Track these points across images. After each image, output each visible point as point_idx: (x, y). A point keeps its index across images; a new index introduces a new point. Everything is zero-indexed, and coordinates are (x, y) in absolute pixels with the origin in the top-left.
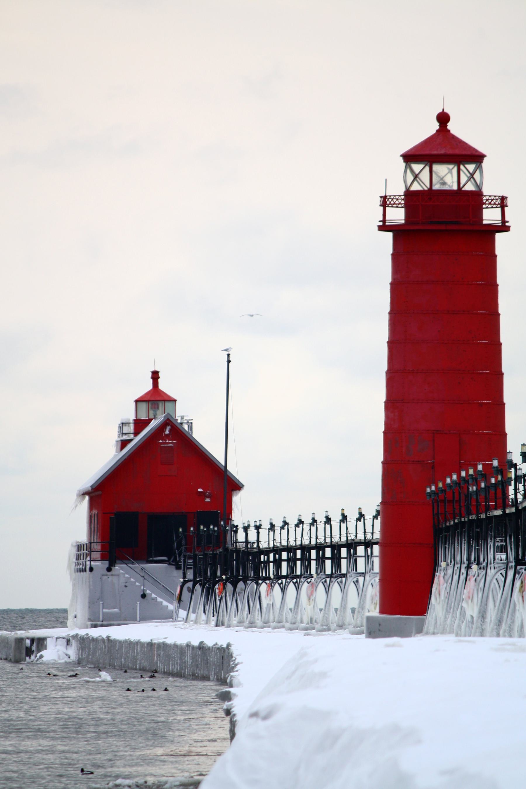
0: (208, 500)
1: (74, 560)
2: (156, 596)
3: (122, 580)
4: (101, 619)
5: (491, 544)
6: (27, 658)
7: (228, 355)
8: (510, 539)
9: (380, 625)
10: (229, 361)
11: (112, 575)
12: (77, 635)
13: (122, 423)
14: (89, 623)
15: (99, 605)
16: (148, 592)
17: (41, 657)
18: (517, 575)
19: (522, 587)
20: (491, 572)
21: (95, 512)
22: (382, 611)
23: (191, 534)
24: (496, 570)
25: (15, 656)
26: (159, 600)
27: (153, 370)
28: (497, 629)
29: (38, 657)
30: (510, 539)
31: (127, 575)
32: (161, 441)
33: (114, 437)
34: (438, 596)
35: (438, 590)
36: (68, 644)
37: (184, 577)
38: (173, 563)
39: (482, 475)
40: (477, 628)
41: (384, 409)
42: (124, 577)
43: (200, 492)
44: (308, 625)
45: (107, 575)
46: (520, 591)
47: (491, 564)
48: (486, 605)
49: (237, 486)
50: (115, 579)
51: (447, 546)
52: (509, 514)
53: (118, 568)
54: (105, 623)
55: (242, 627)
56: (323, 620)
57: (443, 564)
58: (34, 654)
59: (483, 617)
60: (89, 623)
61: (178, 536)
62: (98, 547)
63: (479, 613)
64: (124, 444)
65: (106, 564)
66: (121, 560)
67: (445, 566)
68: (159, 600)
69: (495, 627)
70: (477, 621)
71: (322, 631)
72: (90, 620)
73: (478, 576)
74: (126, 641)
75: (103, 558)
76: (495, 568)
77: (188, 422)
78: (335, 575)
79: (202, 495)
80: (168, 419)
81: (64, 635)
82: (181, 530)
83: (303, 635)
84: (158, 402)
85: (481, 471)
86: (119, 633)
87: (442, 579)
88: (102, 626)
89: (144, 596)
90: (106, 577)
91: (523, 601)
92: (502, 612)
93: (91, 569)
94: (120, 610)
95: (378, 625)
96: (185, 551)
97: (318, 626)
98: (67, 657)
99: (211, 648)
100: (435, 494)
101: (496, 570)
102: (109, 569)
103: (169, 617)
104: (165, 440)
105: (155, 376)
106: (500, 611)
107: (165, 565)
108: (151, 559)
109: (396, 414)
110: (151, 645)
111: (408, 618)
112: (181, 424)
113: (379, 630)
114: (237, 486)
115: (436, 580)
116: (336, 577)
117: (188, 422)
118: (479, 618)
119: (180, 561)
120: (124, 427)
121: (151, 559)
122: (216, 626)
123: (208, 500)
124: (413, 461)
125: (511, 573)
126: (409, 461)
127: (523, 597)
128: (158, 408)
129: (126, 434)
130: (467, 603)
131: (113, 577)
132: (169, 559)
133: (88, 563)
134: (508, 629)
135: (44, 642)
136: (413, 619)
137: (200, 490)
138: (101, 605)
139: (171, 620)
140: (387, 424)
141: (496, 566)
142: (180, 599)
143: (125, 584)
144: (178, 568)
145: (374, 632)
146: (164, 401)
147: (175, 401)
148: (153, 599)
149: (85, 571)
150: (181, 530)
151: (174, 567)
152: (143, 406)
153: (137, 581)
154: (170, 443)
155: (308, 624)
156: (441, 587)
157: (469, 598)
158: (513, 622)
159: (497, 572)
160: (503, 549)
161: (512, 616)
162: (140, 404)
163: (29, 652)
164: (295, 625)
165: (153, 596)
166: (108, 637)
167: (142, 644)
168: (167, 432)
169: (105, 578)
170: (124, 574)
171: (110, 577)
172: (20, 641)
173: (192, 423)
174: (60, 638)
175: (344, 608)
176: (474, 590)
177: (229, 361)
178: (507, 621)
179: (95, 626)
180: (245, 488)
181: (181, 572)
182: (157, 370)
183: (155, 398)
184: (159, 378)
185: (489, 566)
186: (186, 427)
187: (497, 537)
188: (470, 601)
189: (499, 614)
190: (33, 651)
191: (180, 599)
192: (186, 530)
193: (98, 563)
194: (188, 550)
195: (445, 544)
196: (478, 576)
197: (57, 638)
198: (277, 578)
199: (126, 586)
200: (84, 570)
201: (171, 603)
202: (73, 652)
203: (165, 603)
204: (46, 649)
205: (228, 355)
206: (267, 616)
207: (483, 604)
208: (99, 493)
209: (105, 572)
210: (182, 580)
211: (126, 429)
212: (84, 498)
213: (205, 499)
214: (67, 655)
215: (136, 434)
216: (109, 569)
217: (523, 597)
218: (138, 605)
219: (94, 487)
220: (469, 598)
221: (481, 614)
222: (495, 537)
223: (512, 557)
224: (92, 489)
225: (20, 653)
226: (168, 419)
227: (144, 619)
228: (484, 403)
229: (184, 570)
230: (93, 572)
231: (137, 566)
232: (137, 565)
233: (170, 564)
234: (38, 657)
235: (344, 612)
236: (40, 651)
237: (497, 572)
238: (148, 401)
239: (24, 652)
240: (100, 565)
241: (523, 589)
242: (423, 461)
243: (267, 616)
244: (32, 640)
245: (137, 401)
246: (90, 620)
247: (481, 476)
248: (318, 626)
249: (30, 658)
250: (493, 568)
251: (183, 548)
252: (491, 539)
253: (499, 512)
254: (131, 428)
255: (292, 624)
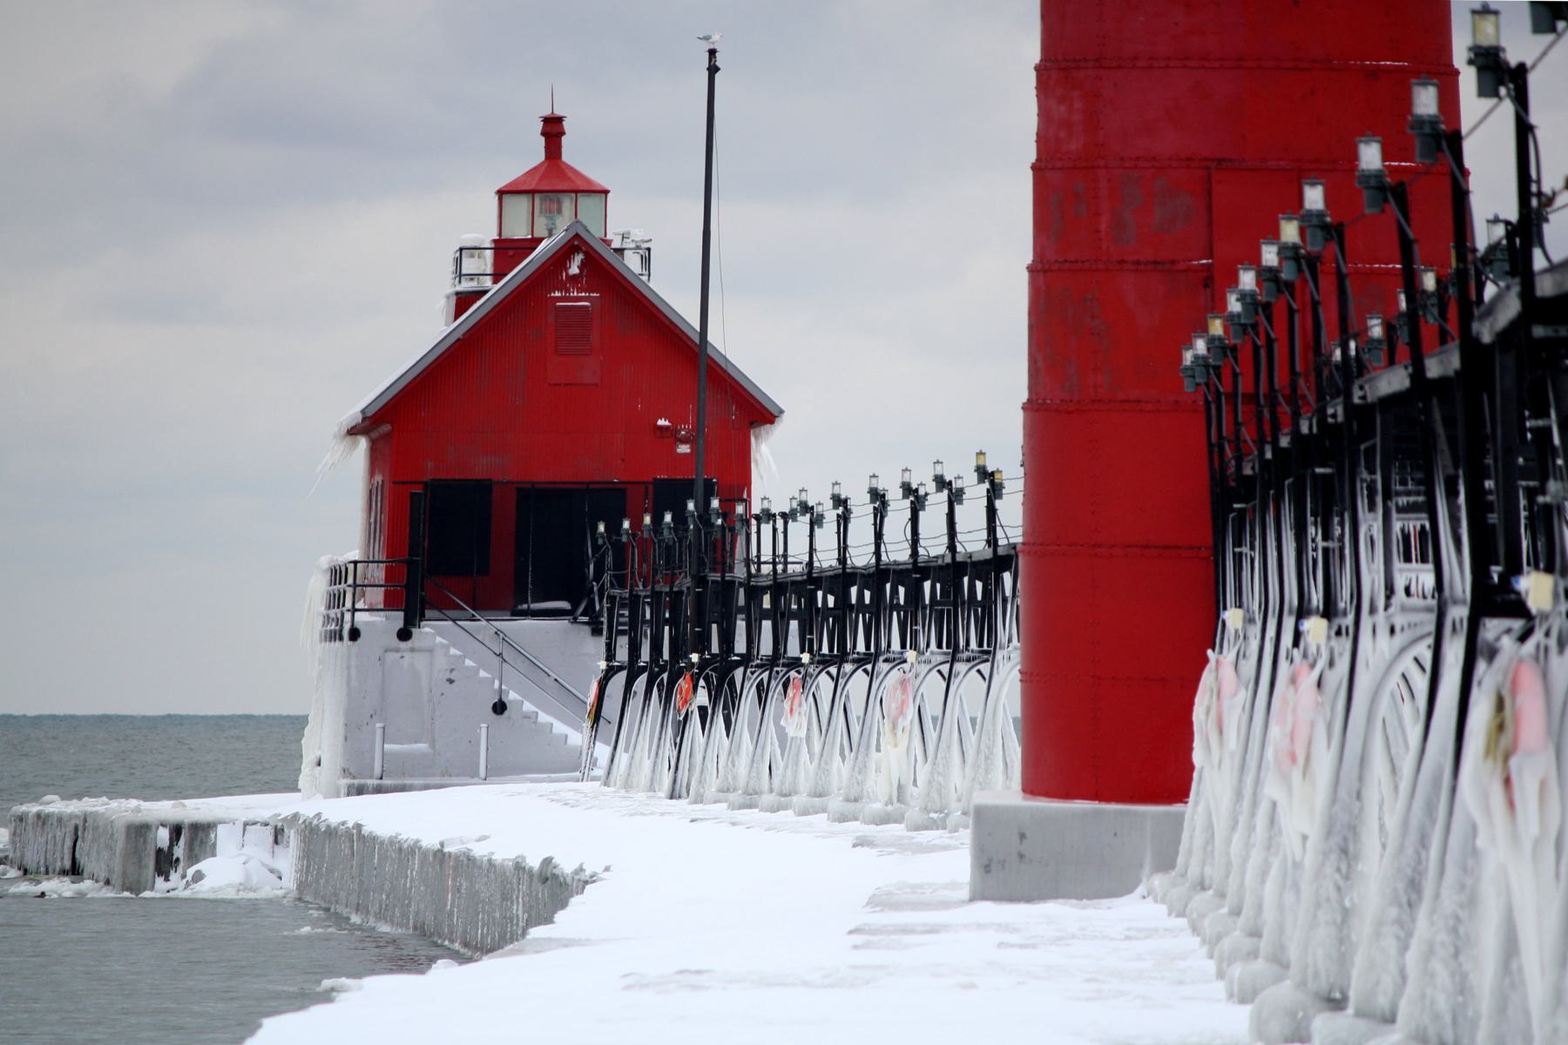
0: (684, 449)
1: (322, 609)
2: (534, 709)
3: (441, 663)
4: (377, 771)
5: (1371, 524)
6: (160, 881)
7: (712, 53)
8: (1452, 494)
9: (1022, 836)
10: (713, 70)
11: (412, 650)
12: (296, 816)
13: (461, 249)
14: (344, 782)
15: (374, 733)
16: (512, 696)
17: (198, 877)
18: (1481, 666)
19: (1501, 727)
20: (1376, 648)
21: (378, 478)
22: (1033, 787)
23: (624, 539)
24: (1400, 639)
25: (124, 873)
26: (544, 718)
27: (547, 112)
28: (1399, 922)
29: (189, 877)
30: (1452, 494)
31: (453, 651)
32: (557, 294)
33: (447, 287)
34: (1214, 737)
35: (1213, 713)
36: (276, 842)
37: (610, 656)
38: (586, 619)
39: (1325, 227)
40: (1318, 906)
41: (1034, 92)
42: (447, 655)
43: (661, 428)
44: (890, 808)
45: (397, 650)
46: (1489, 751)
47: (1373, 610)
48: (1359, 796)
49: (760, 414)
50: (420, 661)
51: (1245, 550)
52: (1443, 381)
53: (430, 632)
54: (386, 782)
55: (725, 805)
56: (928, 794)
57: (1232, 617)
58: (180, 869)
59: (1344, 851)
60: (344, 782)
61: (594, 541)
62: (378, 573)
63: (1329, 832)
64: (463, 301)
65: (397, 619)
66: (440, 610)
67: (1239, 625)
68: (544, 718)
69: (1393, 912)
70: (1318, 873)
71: (926, 828)
72: (346, 772)
73: (1331, 664)
74: (392, 841)
75: (390, 604)
76: (1392, 631)
77: (638, 248)
78: (965, 655)
79: (671, 435)
80: (577, 236)
81: (264, 814)
82: (601, 528)
83: (850, 840)
84: (561, 196)
85: (1320, 214)
86: (396, 817)
87: (1227, 671)
88: (379, 790)
89: (500, 708)
90: (398, 655)
91: (1511, 804)
92: (1424, 842)
93: (355, 634)
94: (433, 744)
95: (1016, 838)
96: (612, 586)
97: (914, 813)
98: (273, 877)
99: (569, 880)
100: (1207, 366)
101: (1400, 639)
102: (404, 635)
103: (571, 765)
104: (567, 290)
105: (553, 129)
106: (1413, 836)
107: (562, 624)
108: (525, 606)
109: (1078, 105)
110: (440, 855)
111: (1128, 812)
112: (620, 251)
113: (1021, 856)
114: (760, 414)
115: (1207, 677)
116: (968, 660)
117: (638, 248)
118: (1326, 854)
119: (600, 613)
120: (465, 261)
121: (525, 606)
122: (672, 797)
123: (684, 449)
124: (1138, 263)
125: (1454, 652)
126: (1122, 262)
127: (1507, 782)
128: (560, 211)
129: (472, 276)
130: (1286, 779)
131: (415, 655)
132: (575, 606)
133: (348, 616)
134: (1443, 937)
135: (208, 835)
136: (1144, 814)
137: (662, 422)
138: (379, 733)
139: (577, 774)
140: (1042, 139)
141: (1399, 621)
142: (597, 716)
143: (448, 675)
144: (597, 632)
145: (1003, 863)
146: (576, 192)
147: (606, 192)
148: (527, 716)
149: (341, 638)
150: (601, 528)
151: (587, 629)
152: (519, 207)
153: (481, 665)
154: (582, 299)
155: (890, 802)
156: (1226, 703)
157: (1293, 758)
158: (1471, 902)
159: (1403, 650)
160: (1426, 547)
161: (1465, 869)
162: (506, 198)
163: (165, 863)
164: (858, 805)
165: (528, 707)
166: (358, 826)
167: (425, 854)
168: (574, 269)
169: (392, 657)
170: (447, 648)
171: (408, 656)
172: (140, 831)
173: (649, 249)
174: (255, 823)
175: (987, 758)
176: (1313, 725)
177: (713, 70)
178: (1437, 895)
179: (360, 791)
180: (785, 417)
181: (602, 642)
182: (558, 112)
183: (553, 180)
184: (563, 133)
185: (1366, 621)
186: (632, 262)
187: (1398, 494)
188: (1296, 774)
189: (1410, 851)
190: (178, 860)
191: (597, 716)
192: (614, 528)
193: (378, 618)
194: (620, 582)
195: (1238, 542)
196: (1331, 664)
197: (246, 824)
198: (819, 662)
199: (451, 681)
200: (336, 636)
201: (578, 728)
202: (288, 861)
203: (560, 728)
204: (214, 855)
205: (712, 53)
206: (789, 772)
207: (1342, 793)
208: (386, 428)
209: (395, 641)
210: (603, 665)
211: (469, 266)
212: (355, 445)
213: (674, 446)
214: (272, 871)
215: (497, 277)
216: (404, 635)
217: (1507, 782)
218: (484, 731)
219: (370, 413)
220: (1293, 758)
221: (1336, 840)
222: (1387, 496)
223: (1460, 580)
224: (364, 419)
225: (140, 865)
226: (577, 236)
227: (499, 770)
228: (1387, 70)
229: (610, 637)
230: (359, 641)
231: (484, 627)
232: (484, 623)
233: (575, 621)
234: (189, 877)
235: (987, 771)
236: (198, 861)
237: (1403, 650)
238: (532, 192)
239: (151, 863)
240: (379, 623)
241: (1505, 741)
242: (1173, 262)
243: (789, 772)
244: (176, 831)
245: (501, 193)
246: (346, 772)
247: (1320, 234)
248: (914, 813)
249: (167, 880)
250: (1383, 631)
251: (607, 578)
252: (1372, 507)
253: (1393, 381)
254: (486, 262)
255: (847, 800)
